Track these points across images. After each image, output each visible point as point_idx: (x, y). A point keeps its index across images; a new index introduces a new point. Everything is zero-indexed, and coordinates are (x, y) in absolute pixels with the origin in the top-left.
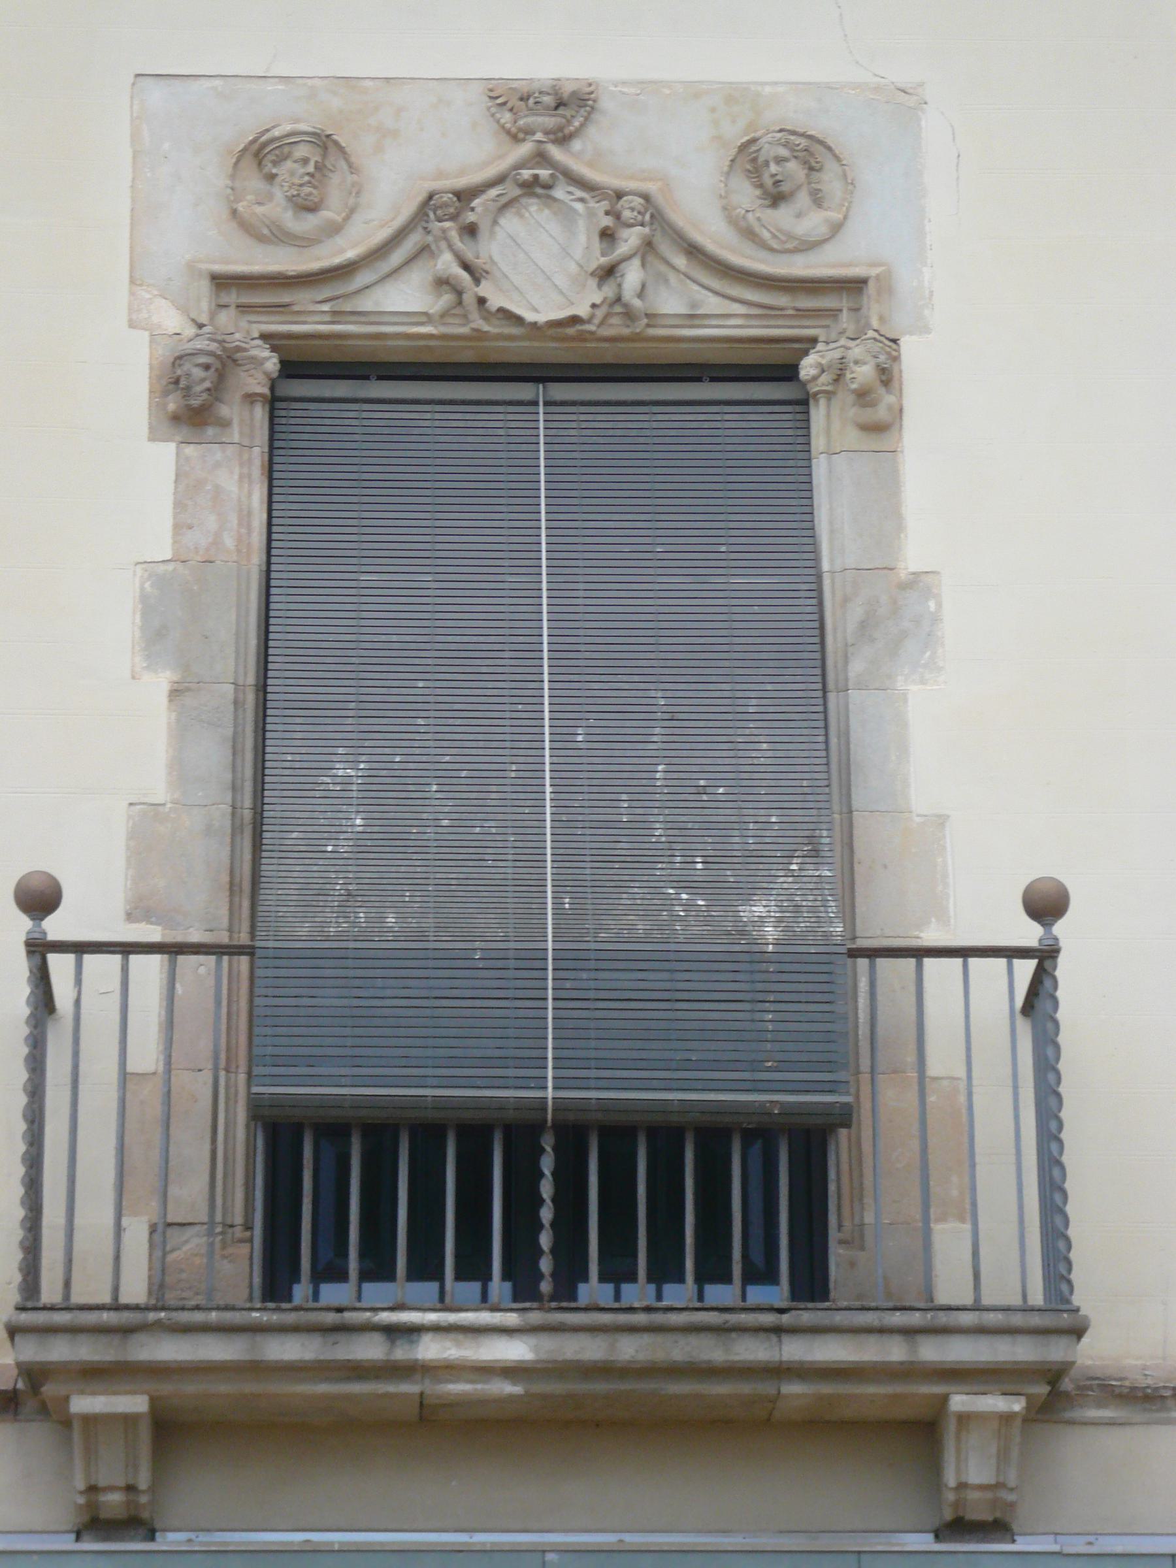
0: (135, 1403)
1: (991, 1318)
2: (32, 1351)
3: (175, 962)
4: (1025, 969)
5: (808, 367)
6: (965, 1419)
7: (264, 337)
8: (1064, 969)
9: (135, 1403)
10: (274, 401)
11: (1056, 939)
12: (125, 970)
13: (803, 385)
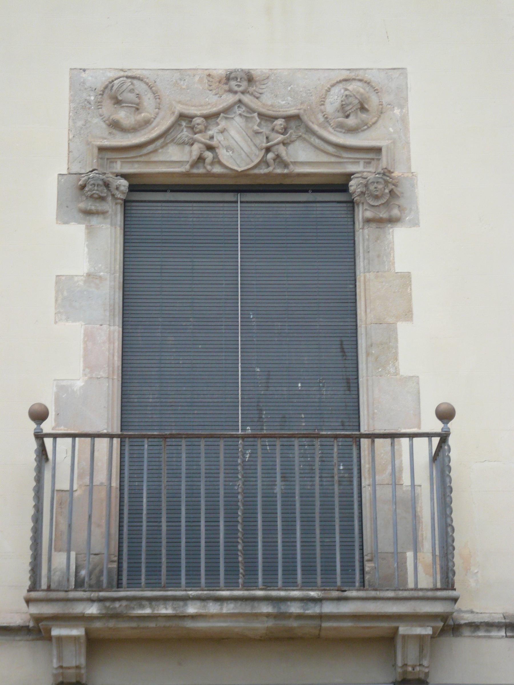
0: (77, 632)
1: (421, 594)
2: (35, 610)
3: (94, 441)
4: (436, 441)
5: (353, 185)
6: (405, 637)
7: (124, 176)
8: (451, 441)
9: (77, 632)
10: (126, 202)
11: (449, 429)
12: (93, 446)
13: (351, 195)
